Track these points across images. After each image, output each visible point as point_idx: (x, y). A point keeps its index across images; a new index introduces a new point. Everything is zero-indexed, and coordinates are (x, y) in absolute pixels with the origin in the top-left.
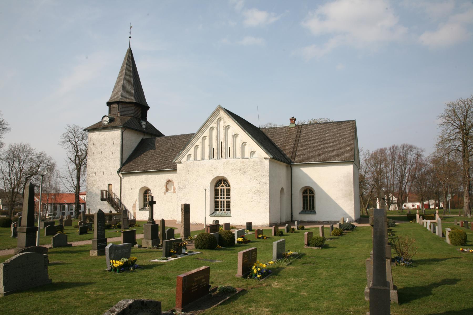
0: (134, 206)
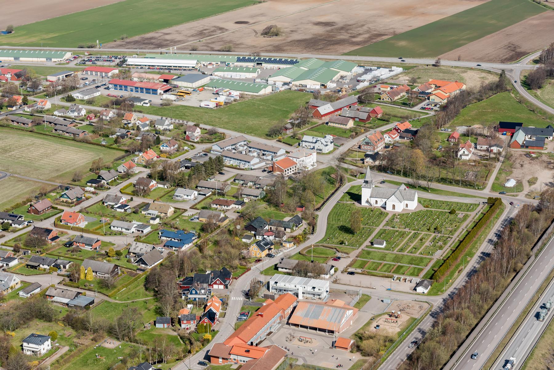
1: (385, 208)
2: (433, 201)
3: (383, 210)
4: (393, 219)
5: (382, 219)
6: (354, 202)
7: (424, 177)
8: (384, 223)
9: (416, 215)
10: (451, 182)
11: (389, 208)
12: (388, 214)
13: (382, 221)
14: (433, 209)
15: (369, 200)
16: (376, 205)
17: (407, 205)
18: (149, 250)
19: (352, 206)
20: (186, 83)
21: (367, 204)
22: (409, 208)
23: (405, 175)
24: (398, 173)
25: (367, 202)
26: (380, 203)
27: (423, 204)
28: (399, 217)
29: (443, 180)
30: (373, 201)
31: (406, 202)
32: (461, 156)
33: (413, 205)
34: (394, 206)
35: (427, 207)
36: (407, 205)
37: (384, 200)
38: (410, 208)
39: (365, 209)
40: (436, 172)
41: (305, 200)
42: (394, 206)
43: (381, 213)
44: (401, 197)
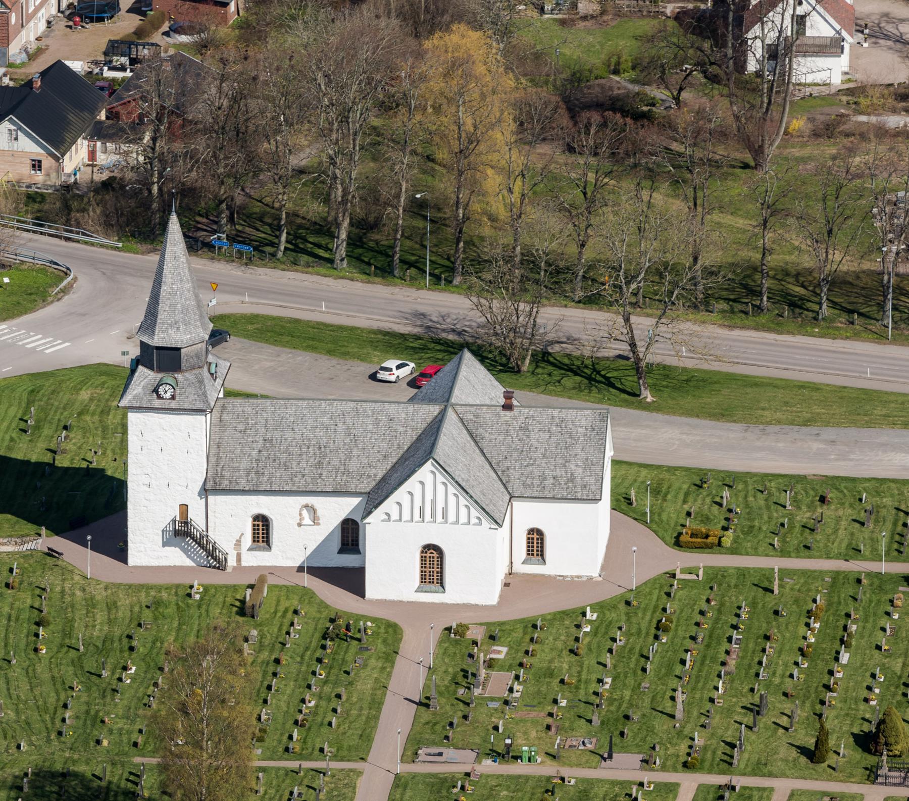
0: (238, 543)
1: (353, 580)
2: (730, 480)
3: (338, 598)
4: (467, 677)
5: (365, 685)
6: (46, 540)
7: (553, 277)
8: (396, 722)
9: (637, 621)
10: (796, 304)
11: (390, 574)
12: (391, 632)
13: (376, 704)
14: (776, 563)
15: (196, 517)
16: (255, 559)
17: (536, 543)
18: (795, 121)
19: (50, 579)
20: (437, 601)
21: (176, 557)
22: (560, 562)
23: (374, 256)
24: (306, 244)
25: (181, 532)
26: (302, 531)
27: (654, 524)
28: (501, 652)
29: (744, 293)
30: (227, 522)
31: (527, 514)
32: (776, 54)
33: (583, 542)
34: (433, 561)
35: (703, 542)
36: (536, 543)
37: (335, 510)
38: (560, 562)
39: (167, 600)
40: (641, 219)
41: (32, 434)
42: (433, 561)
43: (339, 632)
44: (484, 479)
